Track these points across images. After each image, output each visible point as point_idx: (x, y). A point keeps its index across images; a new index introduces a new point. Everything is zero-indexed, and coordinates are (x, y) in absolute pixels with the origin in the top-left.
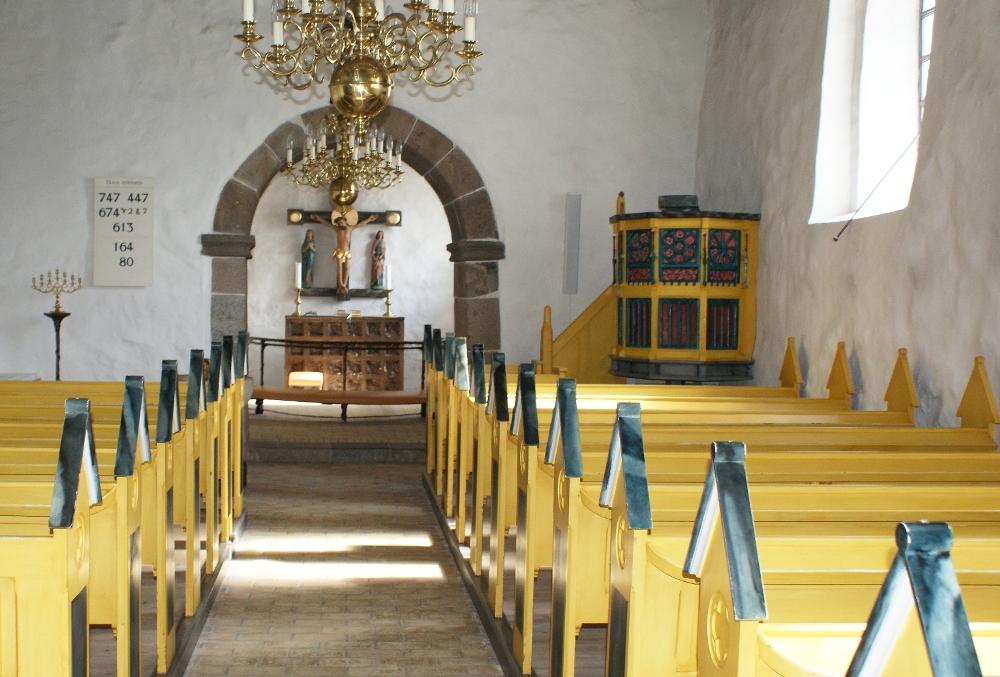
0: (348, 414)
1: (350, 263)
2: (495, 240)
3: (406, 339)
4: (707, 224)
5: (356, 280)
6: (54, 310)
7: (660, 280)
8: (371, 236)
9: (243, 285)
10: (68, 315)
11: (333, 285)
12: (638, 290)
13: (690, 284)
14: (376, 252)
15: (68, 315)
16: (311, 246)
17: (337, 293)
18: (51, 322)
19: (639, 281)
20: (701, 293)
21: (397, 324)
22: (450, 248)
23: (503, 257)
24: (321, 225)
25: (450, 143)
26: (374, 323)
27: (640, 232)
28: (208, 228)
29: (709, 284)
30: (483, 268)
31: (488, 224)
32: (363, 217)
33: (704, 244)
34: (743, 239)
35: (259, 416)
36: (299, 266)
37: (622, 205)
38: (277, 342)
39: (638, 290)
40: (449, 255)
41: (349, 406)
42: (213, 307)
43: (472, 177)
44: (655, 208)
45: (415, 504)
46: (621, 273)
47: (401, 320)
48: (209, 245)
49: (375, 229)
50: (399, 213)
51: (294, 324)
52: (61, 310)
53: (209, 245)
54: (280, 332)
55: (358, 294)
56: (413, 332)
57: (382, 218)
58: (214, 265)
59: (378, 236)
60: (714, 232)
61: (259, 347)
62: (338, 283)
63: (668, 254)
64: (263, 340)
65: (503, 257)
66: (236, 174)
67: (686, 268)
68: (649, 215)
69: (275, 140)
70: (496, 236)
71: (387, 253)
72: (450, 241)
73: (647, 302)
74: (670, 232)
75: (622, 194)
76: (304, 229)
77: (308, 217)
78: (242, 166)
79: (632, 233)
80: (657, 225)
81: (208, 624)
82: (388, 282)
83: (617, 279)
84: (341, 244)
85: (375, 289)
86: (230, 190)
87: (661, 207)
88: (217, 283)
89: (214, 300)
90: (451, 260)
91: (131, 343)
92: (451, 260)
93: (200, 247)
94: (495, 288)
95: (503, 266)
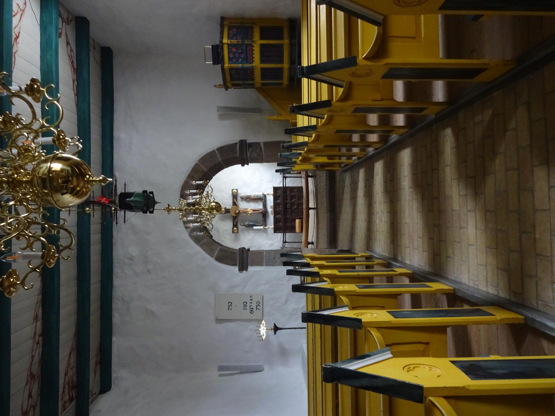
0: (313, 207)
1: (252, 209)
2: (300, 253)
3: (282, 186)
4: (225, 41)
5: (259, 206)
6: (273, 331)
7: (252, 63)
8: (242, 201)
9: (260, 253)
10: (275, 324)
11: (262, 214)
12: (258, 74)
13: (254, 56)
14: (248, 199)
15: (275, 324)
16: (246, 224)
17: (264, 214)
18: (279, 332)
19: (253, 75)
20: (258, 42)
21: (276, 189)
22: (243, 165)
23: (246, 140)
24: (237, 218)
25: (196, 165)
26: (275, 198)
27: (231, 74)
28: (236, 269)
29: (254, 40)
30: (250, 149)
31: (231, 147)
32: (234, 204)
33: (234, 41)
34: (232, 25)
35: (315, 243)
36: (255, 227)
37: (220, 85)
38: (284, 237)
39: (258, 74)
40: (246, 166)
41: (310, 207)
42: (270, 265)
43: (210, 156)
44: (220, 66)
45: (358, 173)
46: (249, 85)
47: (274, 188)
48: (243, 268)
49: (239, 199)
50: (232, 190)
51: (277, 230)
52: (273, 327)
53: (243, 268)
54: (280, 235)
55: (265, 205)
56: (279, 183)
57: (235, 196)
58: (251, 265)
59: (243, 198)
60: (229, 38)
61: (286, 244)
62: (261, 213)
63: (240, 60)
64: (284, 242)
65: (246, 140)
66: (212, 257)
67: (246, 51)
68: (223, 69)
69: (197, 240)
70: (236, 143)
71: (249, 194)
72: (240, 165)
73: (262, 69)
74: (230, 59)
75: (215, 86)
76: (240, 227)
77: (235, 225)
78: (209, 254)
79: (232, 79)
80: (226, 65)
81: (453, 278)
82: (260, 194)
83: (252, 86)
84: (246, 212)
85: (262, 199)
86: (219, 259)
87: (218, 63)
88: (260, 264)
89: (267, 265)
90: (248, 164)
91: (287, 301)
92: (248, 164)
93: (244, 272)
94: (259, 143)
95: (249, 141)
